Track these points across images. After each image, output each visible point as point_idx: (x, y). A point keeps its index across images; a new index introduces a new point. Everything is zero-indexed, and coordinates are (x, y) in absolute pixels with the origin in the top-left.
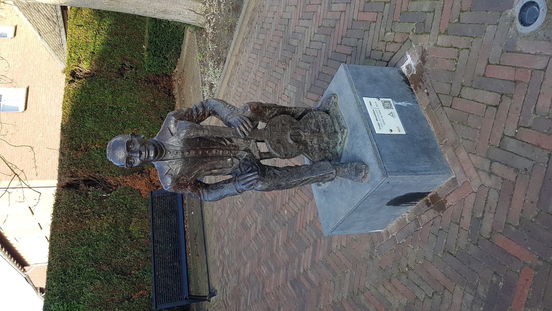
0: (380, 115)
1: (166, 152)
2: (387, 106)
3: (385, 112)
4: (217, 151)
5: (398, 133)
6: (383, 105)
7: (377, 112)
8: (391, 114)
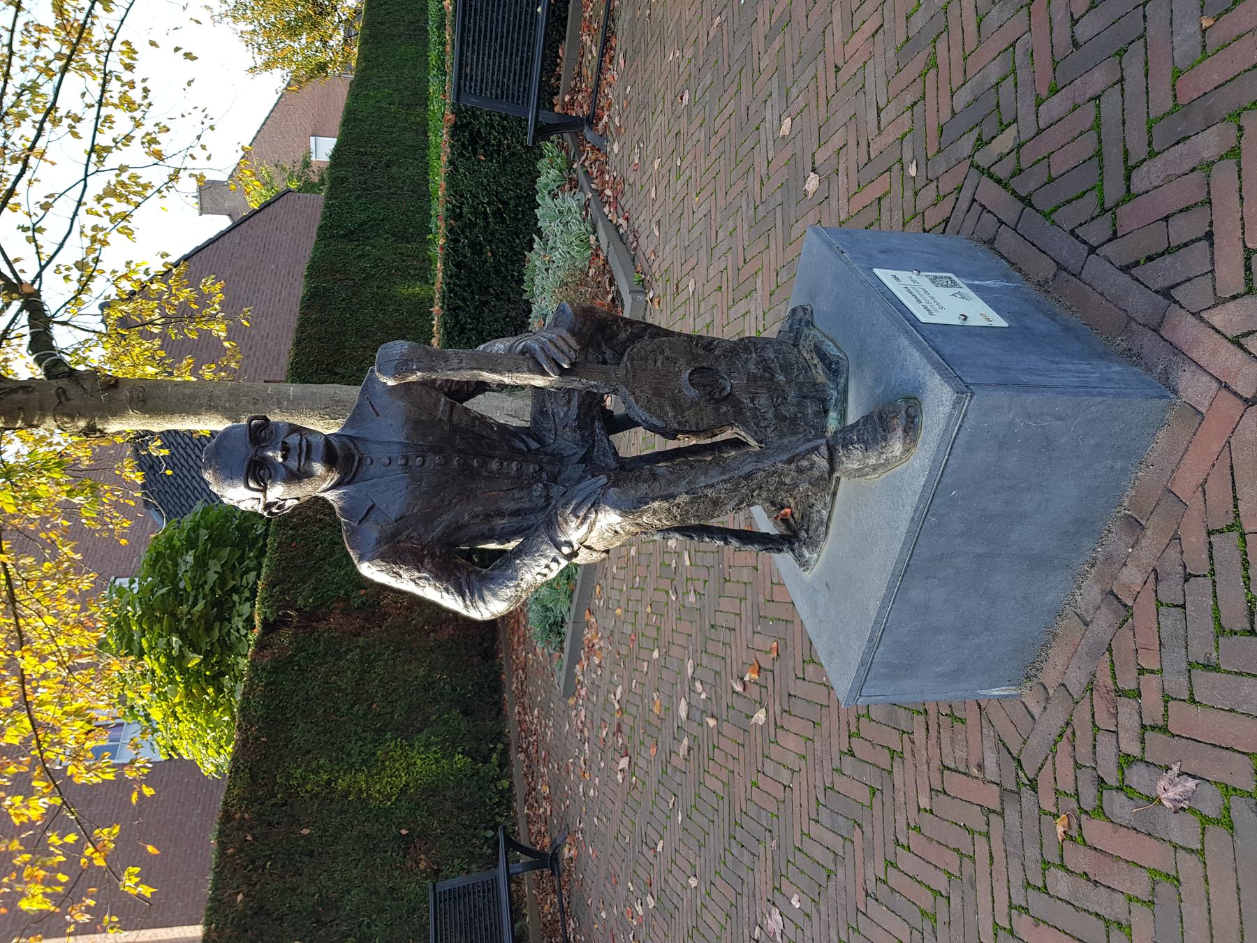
4: (502, 464)
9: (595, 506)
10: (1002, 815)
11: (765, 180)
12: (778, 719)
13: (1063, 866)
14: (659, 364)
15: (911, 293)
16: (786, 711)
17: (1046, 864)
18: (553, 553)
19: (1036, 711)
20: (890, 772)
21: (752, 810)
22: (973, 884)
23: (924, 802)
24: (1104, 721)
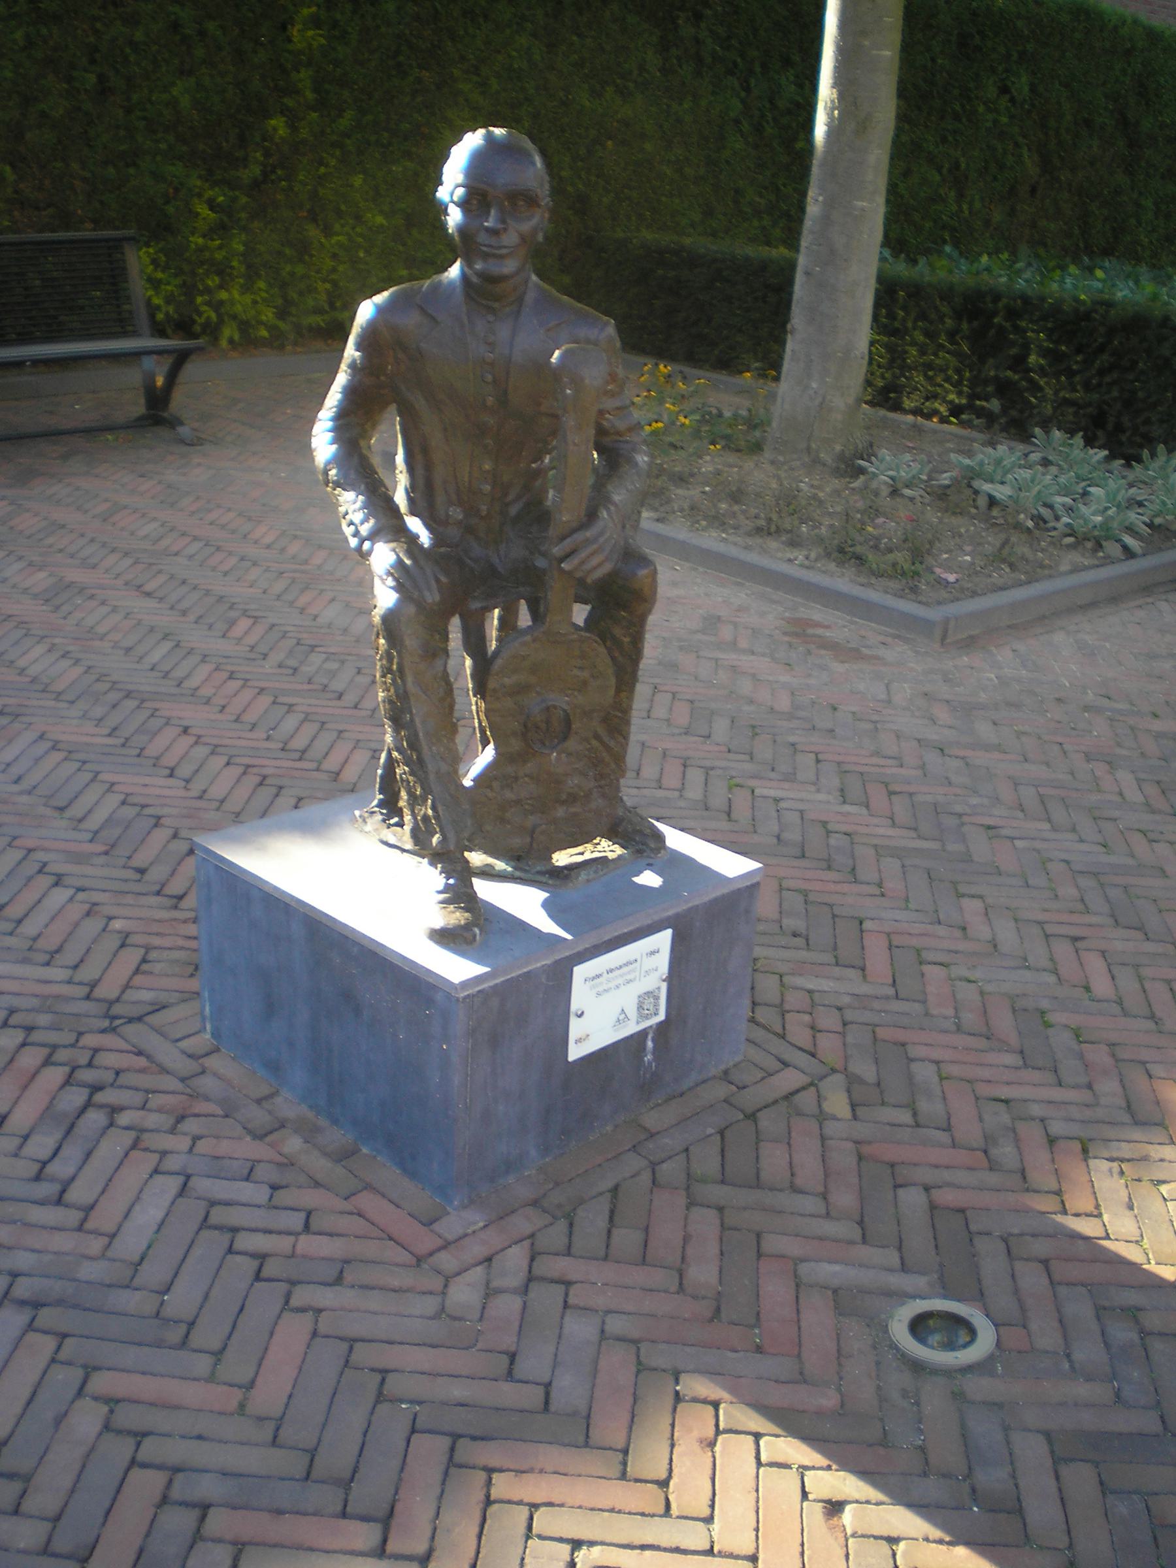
0: (620, 981)
1: (924, 627)
2: (645, 1000)
3: (627, 998)
5: (573, 1035)
6: (648, 994)
7: (629, 972)
8: (620, 1021)
9: (399, 588)
10: (88, 997)
11: (991, 833)
12: (255, 770)
13: (24, 1044)
14: (576, 672)
15: (626, 964)
16: (96, 776)
17: (29, 1029)
18: (365, 530)
19: (184, 1044)
20: (158, 893)
21: (155, 723)
22: (25, 961)
23: (117, 925)
24: (156, 1101)
